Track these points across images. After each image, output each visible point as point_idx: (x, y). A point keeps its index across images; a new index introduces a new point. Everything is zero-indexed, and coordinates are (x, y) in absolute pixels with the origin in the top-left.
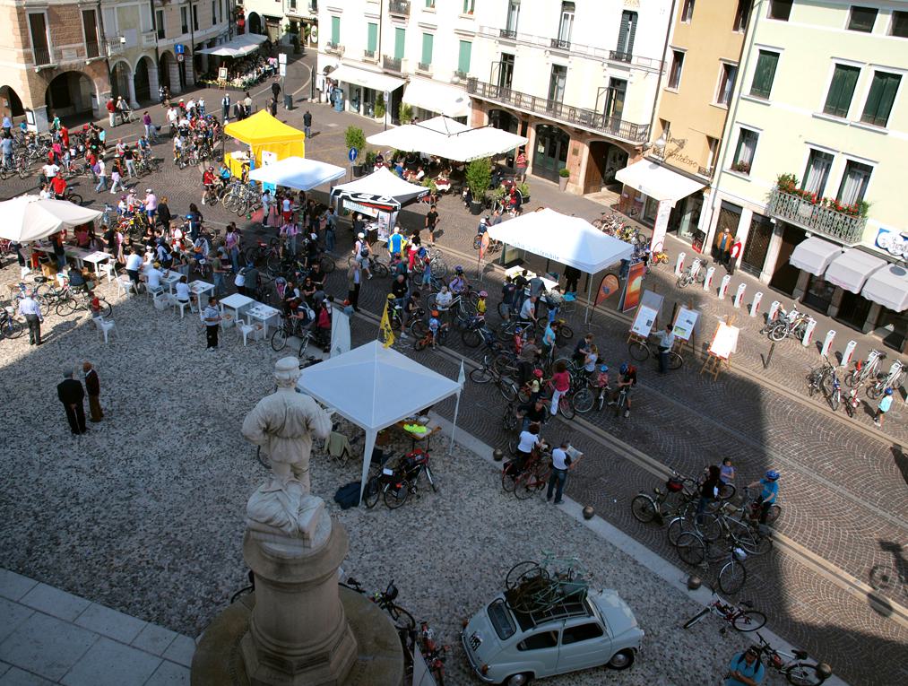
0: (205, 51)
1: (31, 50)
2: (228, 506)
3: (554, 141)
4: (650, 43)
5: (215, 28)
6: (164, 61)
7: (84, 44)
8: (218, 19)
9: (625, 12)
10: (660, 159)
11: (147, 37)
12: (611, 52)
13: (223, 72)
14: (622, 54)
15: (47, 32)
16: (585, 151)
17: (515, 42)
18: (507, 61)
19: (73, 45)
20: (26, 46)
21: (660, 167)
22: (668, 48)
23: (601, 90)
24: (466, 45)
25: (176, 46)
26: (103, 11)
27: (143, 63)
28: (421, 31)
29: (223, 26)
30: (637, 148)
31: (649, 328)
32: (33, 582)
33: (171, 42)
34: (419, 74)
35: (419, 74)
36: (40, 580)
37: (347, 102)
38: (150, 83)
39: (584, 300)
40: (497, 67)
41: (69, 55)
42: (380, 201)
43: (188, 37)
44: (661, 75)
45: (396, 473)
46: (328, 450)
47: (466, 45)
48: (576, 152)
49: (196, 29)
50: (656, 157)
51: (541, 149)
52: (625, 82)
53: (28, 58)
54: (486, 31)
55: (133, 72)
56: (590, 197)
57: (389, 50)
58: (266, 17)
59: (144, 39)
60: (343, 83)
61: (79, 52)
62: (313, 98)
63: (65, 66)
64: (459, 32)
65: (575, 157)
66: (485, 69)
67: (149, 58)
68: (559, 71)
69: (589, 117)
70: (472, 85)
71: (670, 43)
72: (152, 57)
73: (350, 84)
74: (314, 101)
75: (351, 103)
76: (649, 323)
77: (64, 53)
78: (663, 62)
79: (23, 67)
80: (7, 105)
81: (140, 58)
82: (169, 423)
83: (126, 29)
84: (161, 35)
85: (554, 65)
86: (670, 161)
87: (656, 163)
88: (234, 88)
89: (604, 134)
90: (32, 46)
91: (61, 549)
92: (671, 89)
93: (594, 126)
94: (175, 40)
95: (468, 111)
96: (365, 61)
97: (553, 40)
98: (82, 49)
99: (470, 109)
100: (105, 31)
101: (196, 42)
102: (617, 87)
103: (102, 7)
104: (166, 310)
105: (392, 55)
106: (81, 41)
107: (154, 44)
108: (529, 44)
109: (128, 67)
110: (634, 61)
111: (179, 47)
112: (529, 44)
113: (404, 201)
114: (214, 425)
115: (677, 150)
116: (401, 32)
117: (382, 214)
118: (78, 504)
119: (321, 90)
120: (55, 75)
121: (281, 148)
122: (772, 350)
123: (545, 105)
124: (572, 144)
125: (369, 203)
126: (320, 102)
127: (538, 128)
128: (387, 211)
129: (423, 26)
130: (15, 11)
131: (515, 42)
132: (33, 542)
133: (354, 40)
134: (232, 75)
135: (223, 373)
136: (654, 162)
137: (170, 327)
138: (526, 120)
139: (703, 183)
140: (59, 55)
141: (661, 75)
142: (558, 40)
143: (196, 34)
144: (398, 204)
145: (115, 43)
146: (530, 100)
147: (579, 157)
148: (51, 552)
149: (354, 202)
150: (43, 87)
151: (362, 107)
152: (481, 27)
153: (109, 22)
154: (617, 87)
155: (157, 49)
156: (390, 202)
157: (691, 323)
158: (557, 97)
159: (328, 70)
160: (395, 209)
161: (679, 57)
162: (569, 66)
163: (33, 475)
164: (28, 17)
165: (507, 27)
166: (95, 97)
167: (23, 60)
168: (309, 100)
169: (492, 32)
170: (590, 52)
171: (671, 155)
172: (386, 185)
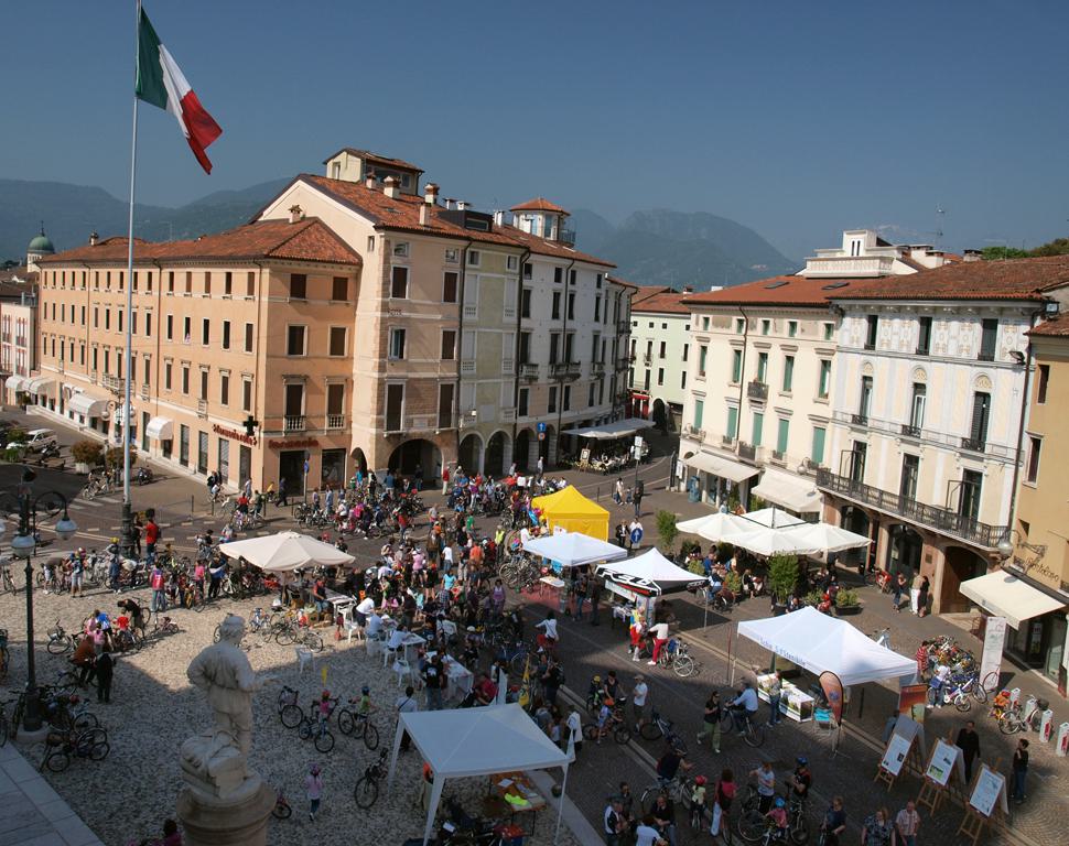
0: (573, 432)
1: (384, 417)
2: (298, 829)
3: (909, 544)
4: (1002, 430)
5: (591, 410)
6: (524, 438)
7: (437, 415)
8: (596, 400)
9: (978, 394)
10: (1021, 570)
11: (506, 413)
12: (964, 439)
13: (585, 454)
15: (403, 403)
16: (940, 559)
17: (865, 428)
19: (426, 415)
20: (380, 412)
21: (1019, 581)
22: (1025, 436)
23: (953, 485)
24: (819, 433)
26: (462, 386)
27: (499, 438)
28: (810, 425)
29: (606, 408)
30: (992, 555)
31: (900, 764)
32: (97, 838)
33: (534, 419)
34: (774, 464)
35: (774, 464)
36: (101, 839)
37: (704, 493)
39: (848, 731)
40: (847, 456)
41: (419, 423)
42: (639, 584)
43: (554, 416)
44: (1017, 466)
46: (422, 802)
47: (819, 433)
48: (929, 559)
49: (567, 408)
50: (1017, 568)
51: (895, 554)
52: (980, 475)
53: (379, 424)
54: (839, 417)
55: (485, 446)
56: (944, 617)
57: (746, 436)
58: (670, 404)
59: (502, 414)
60: (702, 471)
61: (431, 422)
62: (672, 486)
63: (415, 434)
64: (813, 418)
65: (928, 565)
66: (836, 460)
68: (911, 462)
69: (941, 516)
70: (823, 477)
71: (1026, 428)
73: (709, 474)
74: (672, 489)
76: (900, 757)
77: (415, 422)
78: (1019, 451)
79: (374, 431)
80: (357, 465)
82: (302, 749)
83: (484, 403)
84: (523, 412)
85: (906, 455)
86: (1032, 573)
87: (1015, 575)
88: (594, 471)
89: (953, 537)
91: (136, 821)
92: (1028, 483)
93: (948, 528)
94: (538, 417)
95: (821, 508)
96: (723, 448)
97: (904, 426)
98: (434, 419)
99: (822, 505)
100: (461, 404)
102: (972, 481)
103: (461, 382)
104: (375, 657)
105: (749, 442)
106: (435, 412)
108: (880, 431)
110: (988, 449)
112: (880, 431)
113: (666, 587)
114: (341, 760)
115: (1037, 559)
116: (759, 417)
117: (641, 599)
118: (177, 791)
119: (681, 477)
120: (403, 441)
121: (576, 524)
123: (897, 501)
124: (926, 549)
125: (628, 585)
126: (679, 491)
127: (891, 530)
128: (645, 595)
129: (779, 410)
130: (376, 381)
131: (865, 428)
132: (120, 810)
133: (715, 424)
134: (594, 455)
135: (386, 719)
136: (1013, 574)
137: (367, 672)
138: (878, 520)
139: (1061, 601)
140: (410, 423)
141: (1017, 466)
142: (911, 427)
143: (565, 415)
144: (658, 589)
145: (468, 416)
146: (877, 494)
147: (935, 564)
148: (127, 821)
149: (616, 583)
150: (388, 451)
151: (718, 498)
152: (835, 412)
153: (467, 396)
154: (972, 481)
156: (649, 585)
157: (949, 763)
158: (914, 493)
159: (689, 455)
160: (654, 594)
161: (1036, 443)
162: (921, 456)
163: (160, 760)
164: (387, 387)
165: (861, 412)
166: (440, 466)
167: (374, 425)
168: (668, 488)
169: (893, 427)
170: (943, 440)
171: (1031, 566)
172: (653, 567)
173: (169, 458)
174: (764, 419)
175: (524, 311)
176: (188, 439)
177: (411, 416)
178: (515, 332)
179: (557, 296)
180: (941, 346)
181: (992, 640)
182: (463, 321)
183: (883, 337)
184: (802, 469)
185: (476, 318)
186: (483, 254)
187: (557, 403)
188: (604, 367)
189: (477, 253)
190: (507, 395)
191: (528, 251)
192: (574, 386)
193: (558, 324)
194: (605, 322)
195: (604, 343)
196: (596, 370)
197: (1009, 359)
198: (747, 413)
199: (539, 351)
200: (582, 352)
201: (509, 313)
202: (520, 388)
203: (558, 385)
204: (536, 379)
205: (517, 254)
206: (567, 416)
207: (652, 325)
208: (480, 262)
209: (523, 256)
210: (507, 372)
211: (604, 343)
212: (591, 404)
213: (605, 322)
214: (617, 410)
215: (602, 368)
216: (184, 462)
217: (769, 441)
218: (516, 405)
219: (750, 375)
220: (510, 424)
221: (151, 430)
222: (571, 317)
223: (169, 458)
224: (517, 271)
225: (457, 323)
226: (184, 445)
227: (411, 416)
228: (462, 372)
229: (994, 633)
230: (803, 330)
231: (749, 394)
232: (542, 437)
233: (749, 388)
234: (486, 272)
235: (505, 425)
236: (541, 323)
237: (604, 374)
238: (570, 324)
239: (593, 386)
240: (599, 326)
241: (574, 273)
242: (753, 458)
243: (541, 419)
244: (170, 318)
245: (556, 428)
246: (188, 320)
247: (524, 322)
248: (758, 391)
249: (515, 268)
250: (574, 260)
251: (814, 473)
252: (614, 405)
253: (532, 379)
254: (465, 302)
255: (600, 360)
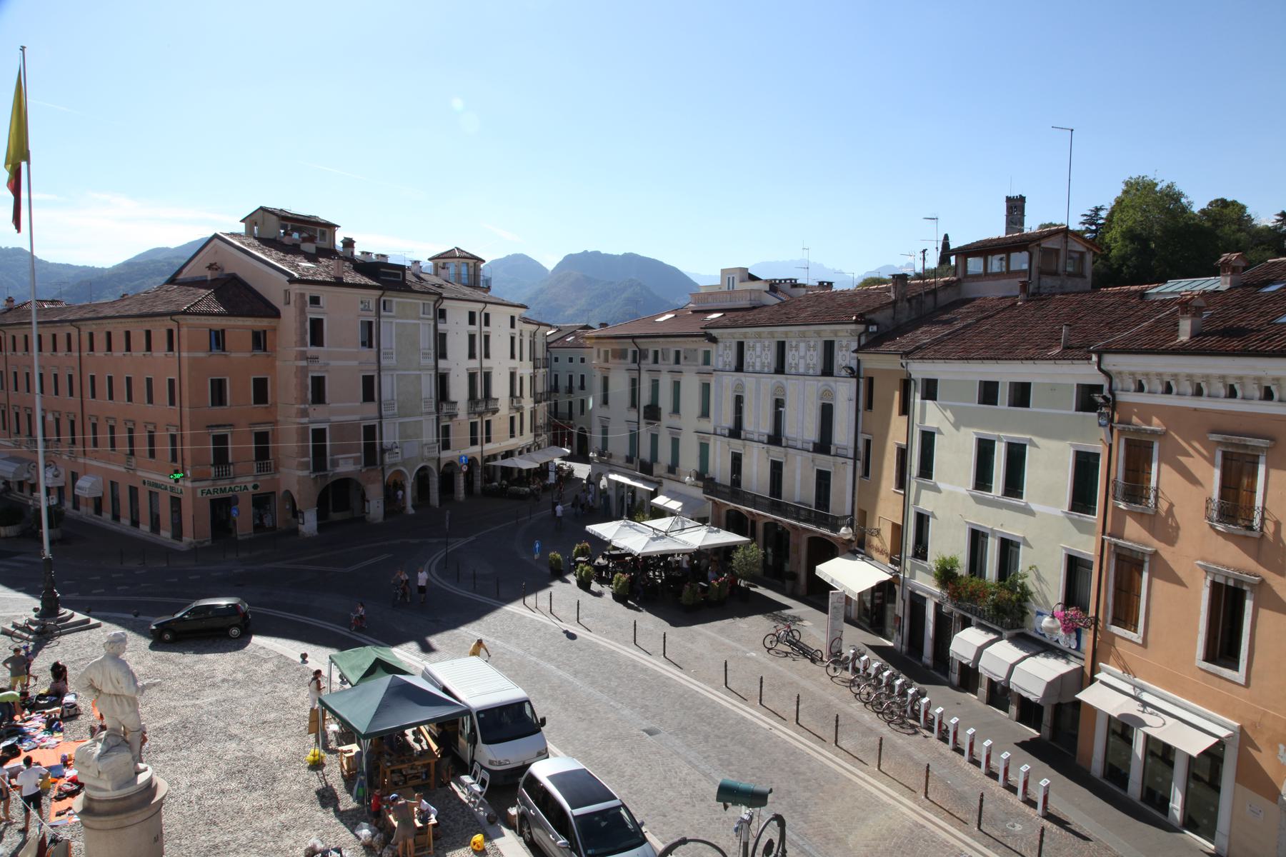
5: (513, 441)
6: (448, 474)
14: (823, 445)
18: (776, 468)
25: (460, 457)
27: (423, 475)
38: (431, 491)
43: (477, 449)
45: (343, 812)
49: (488, 440)
59: (426, 450)
61: (356, 461)
66: (720, 468)
67: (431, 469)
72: (433, 466)
75: (338, 466)
77: (341, 462)
80: (288, 507)
81: (415, 471)
84: (446, 446)
90: (311, 456)
98: (360, 457)
101: (485, 454)
102: (823, 479)
107: (435, 454)
109: (406, 476)
111: (464, 458)
122: (881, 744)
154: (823, 479)
155: (439, 459)
173: (101, 515)
174: (660, 438)
175: (441, 352)
176: (118, 495)
177: (336, 457)
178: (433, 373)
179: (472, 338)
180: (766, 364)
181: (835, 610)
182: (382, 366)
183: (748, 360)
184: (24, 439)
185: (394, 361)
186: (397, 302)
187: (479, 436)
188: (523, 400)
189: (391, 301)
190: (429, 434)
191: (441, 297)
192: (494, 419)
193: (474, 364)
194: (521, 359)
195: (521, 379)
196: (515, 404)
197: (844, 373)
198: (645, 432)
199: (459, 390)
200: (500, 389)
201: (426, 355)
202: (442, 424)
203: (479, 420)
204: (456, 415)
205: (430, 301)
206: (490, 448)
207: (571, 360)
208: (394, 309)
209: (436, 302)
210: (427, 410)
211: (521, 379)
212: (512, 436)
213: (521, 359)
214: (539, 440)
215: (520, 402)
216: (116, 517)
217: (665, 456)
218: (438, 436)
219: (645, 399)
220: (433, 459)
221: (79, 488)
222: (487, 356)
223: (101, 515)
224: (432, 316)
225: (375, 367)
226: (115, 500)
227: (336, 457)
228: (383, 412)
229: (836, 605)
230: (686, 358)
231: (645, 418)
232: (465, 469)
233: (645, 412)
234: (401, 318)
235: (430, 459)
236: (458, 365)
237: (522, 408)
238: (486, 363)
239: (512, 419)
240: (516, 363)
241: (487, 316)
242: (651, 474)
243: (463, 452)
244: (93, 378)
245: (479, 459)
246: (110, 378)
247: (442, 363)
248: (653, 413)
249: (429, 314)
250: (486, 303)
251: (701, 484)
252: (536, 436)
253: (452, 416)
254: (382, 348)
255: (518, 394)
